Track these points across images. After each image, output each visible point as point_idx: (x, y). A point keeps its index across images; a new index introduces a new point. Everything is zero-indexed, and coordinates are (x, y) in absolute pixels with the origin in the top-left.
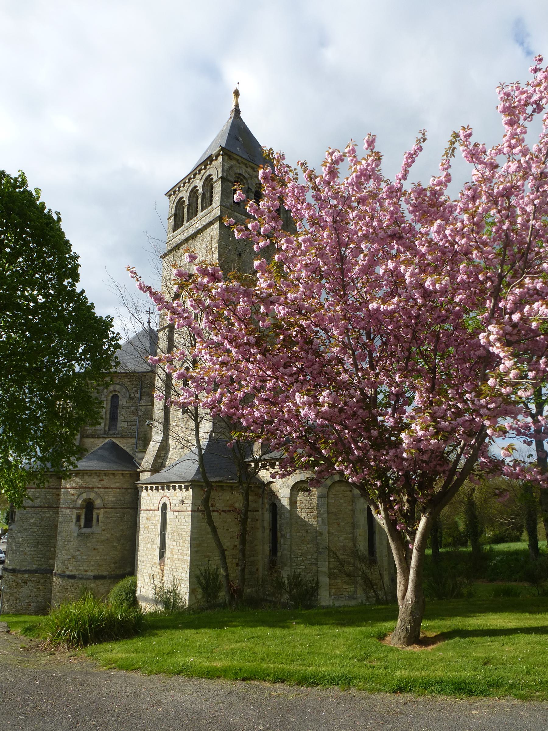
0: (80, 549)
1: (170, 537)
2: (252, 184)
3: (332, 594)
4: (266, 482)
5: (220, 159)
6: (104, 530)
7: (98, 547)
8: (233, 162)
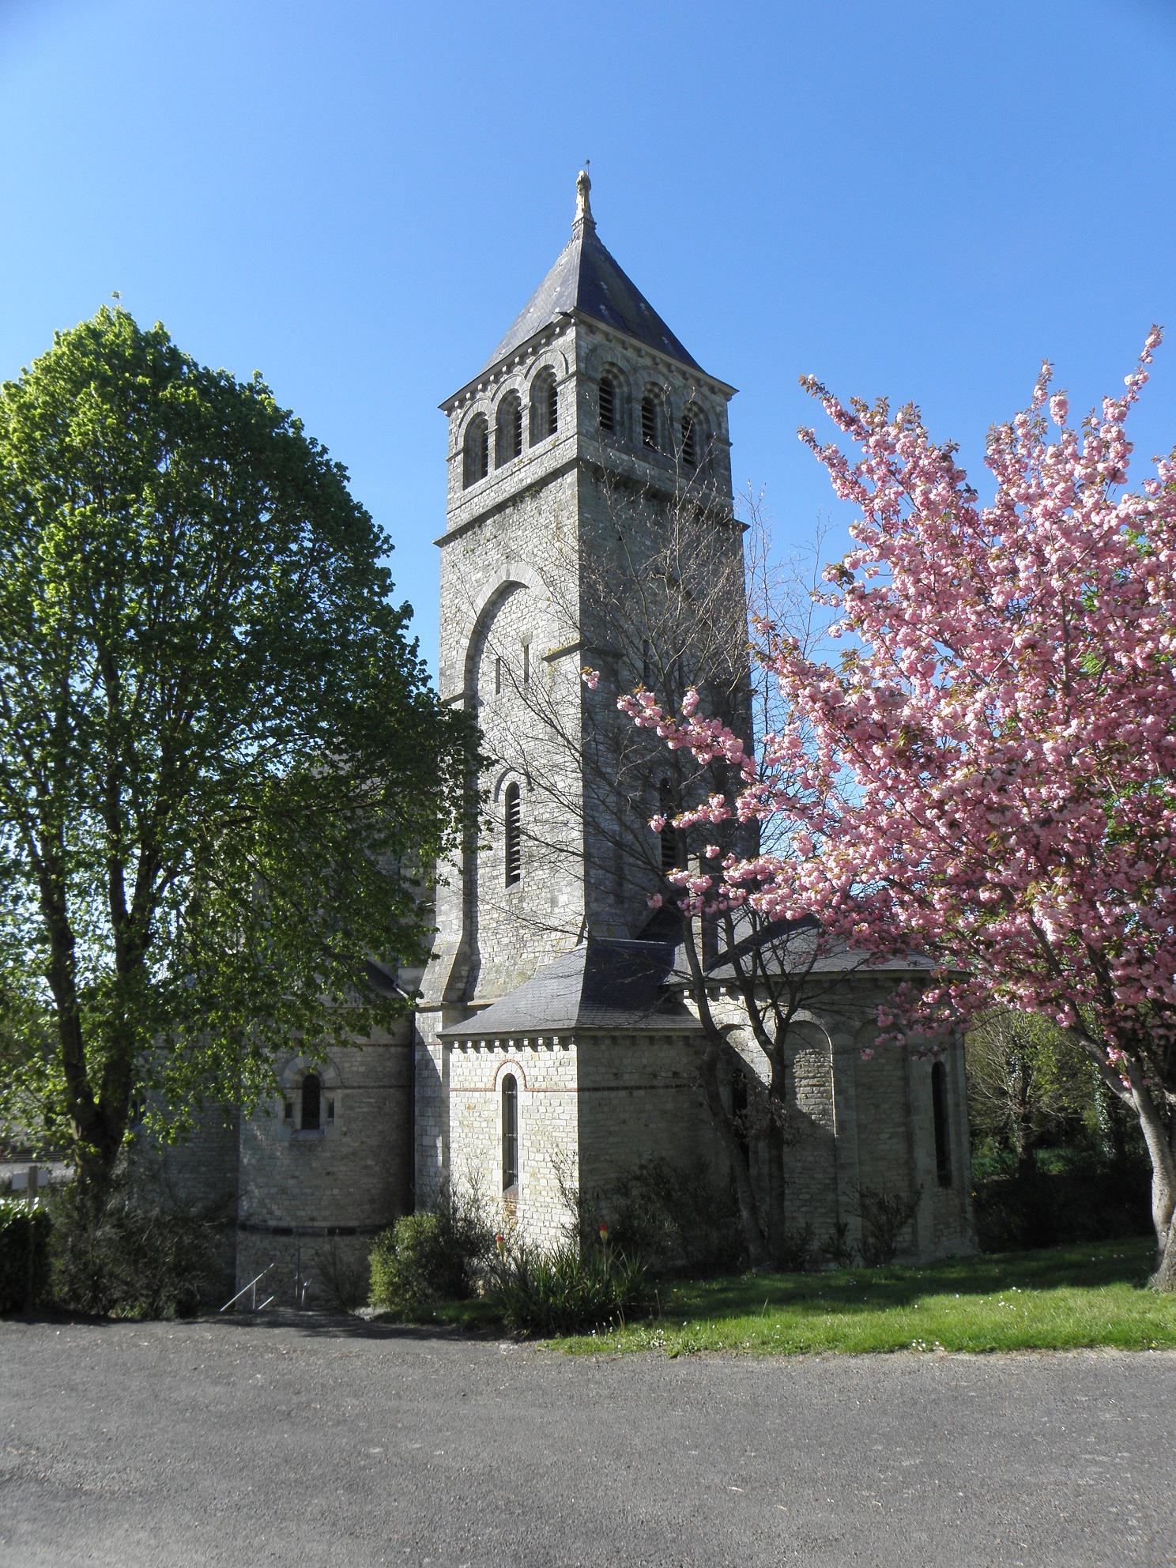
0: (297, 1174)
1: (528, 1143)
4: (719, 1027)
5: (571, 333)
6: (345, 1134)
7: (336, 1169)
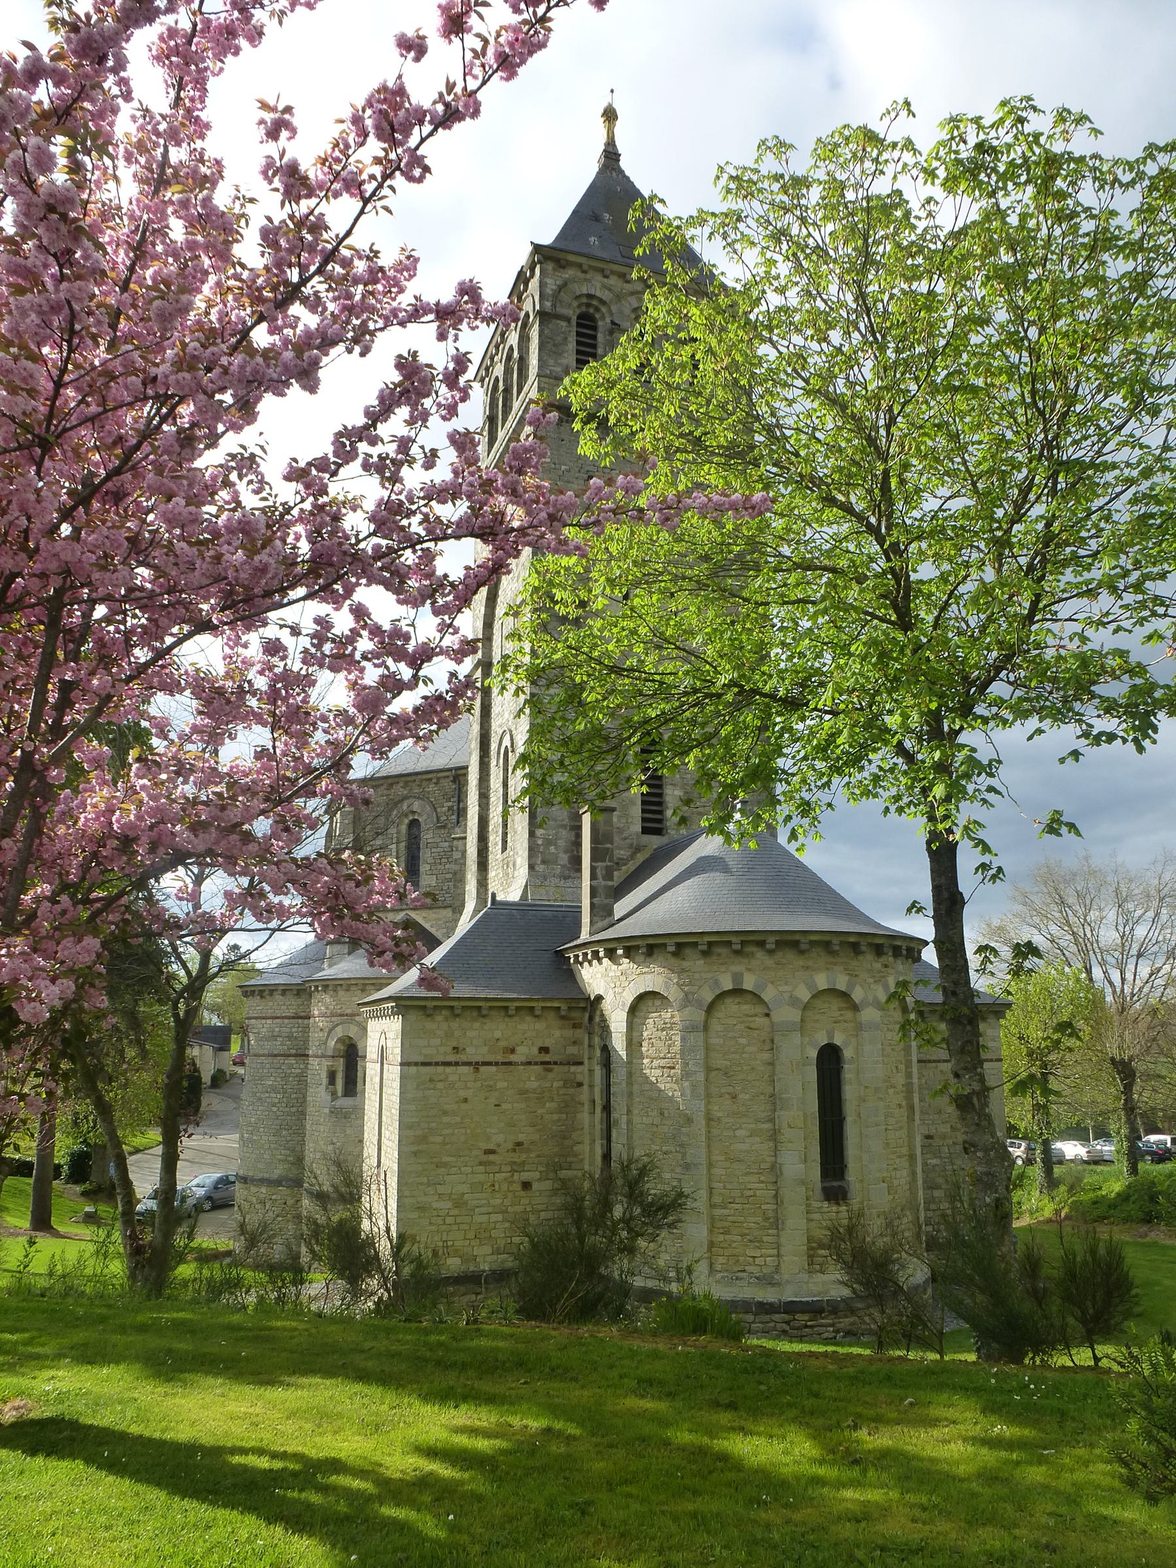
2: (621, 312)
3: (719, 1267)
8: (569, 273)
